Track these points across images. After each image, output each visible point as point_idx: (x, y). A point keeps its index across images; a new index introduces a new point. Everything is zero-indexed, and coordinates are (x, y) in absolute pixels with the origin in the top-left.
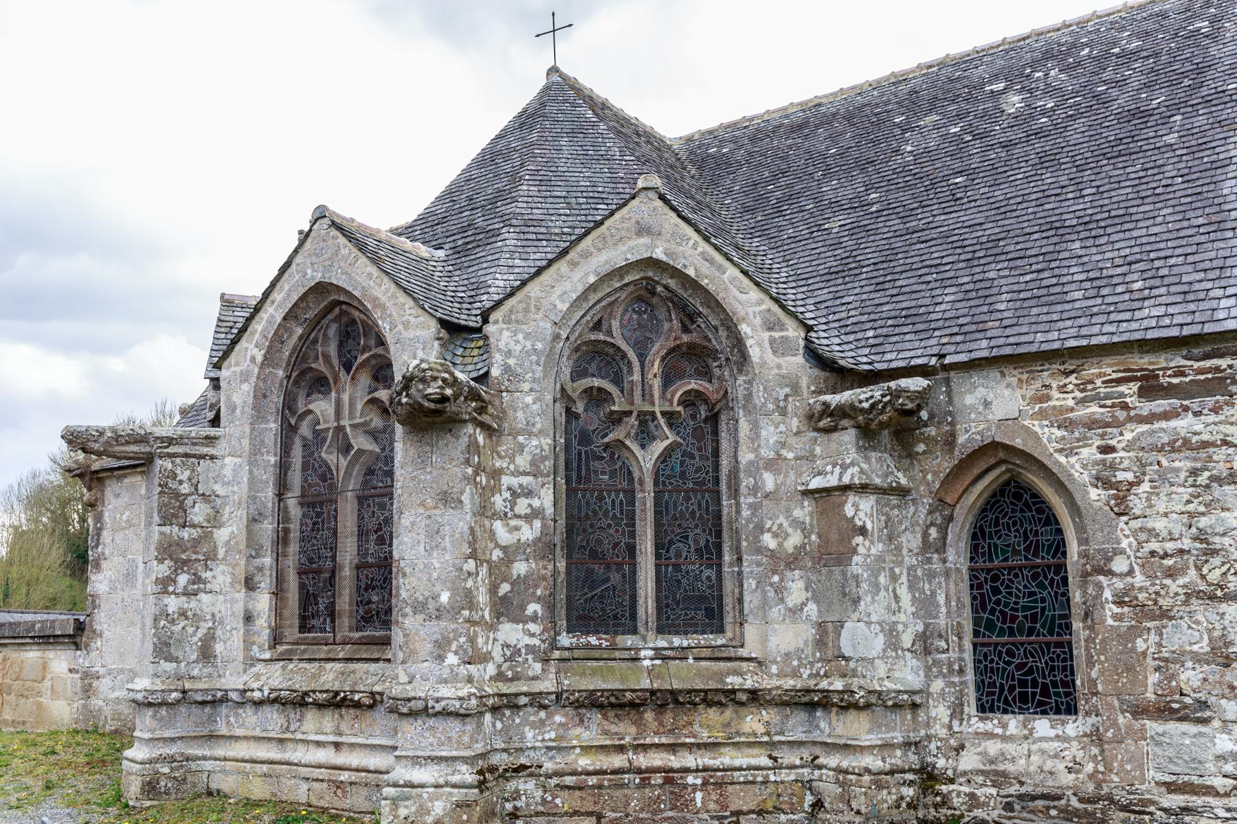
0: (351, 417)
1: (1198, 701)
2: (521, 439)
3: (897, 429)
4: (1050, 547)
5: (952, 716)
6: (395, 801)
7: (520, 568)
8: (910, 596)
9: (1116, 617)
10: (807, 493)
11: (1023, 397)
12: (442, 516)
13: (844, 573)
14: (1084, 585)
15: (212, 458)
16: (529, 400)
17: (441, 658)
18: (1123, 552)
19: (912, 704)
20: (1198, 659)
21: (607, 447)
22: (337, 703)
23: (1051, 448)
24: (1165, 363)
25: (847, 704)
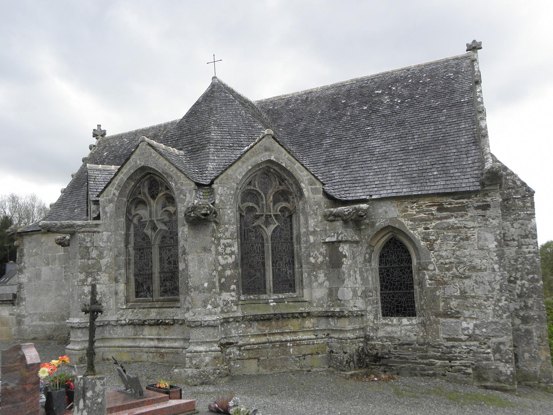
0: (157, 216)
1: (456, 311)
2: (227, 226)
3: (357, 221)
4: (406, 260)
5: (374, 319)
6: (191, 359)
7: (228, 273)
8: (360, 278)
9: (429, 284)
10: (325, 243)
11: (399, 210)
12: (204, 255)
13: (339, 271)
14: (418, 274)
15: (98, 232)
16: (229, 212)
17: (205, 306)
18: (431, 263)
19: (361, 315)
20: (457, 297)
21: (254, 227)
22: (158, 323)
23: (408, 227)
24: (447, 202)
25: (341, 316)
